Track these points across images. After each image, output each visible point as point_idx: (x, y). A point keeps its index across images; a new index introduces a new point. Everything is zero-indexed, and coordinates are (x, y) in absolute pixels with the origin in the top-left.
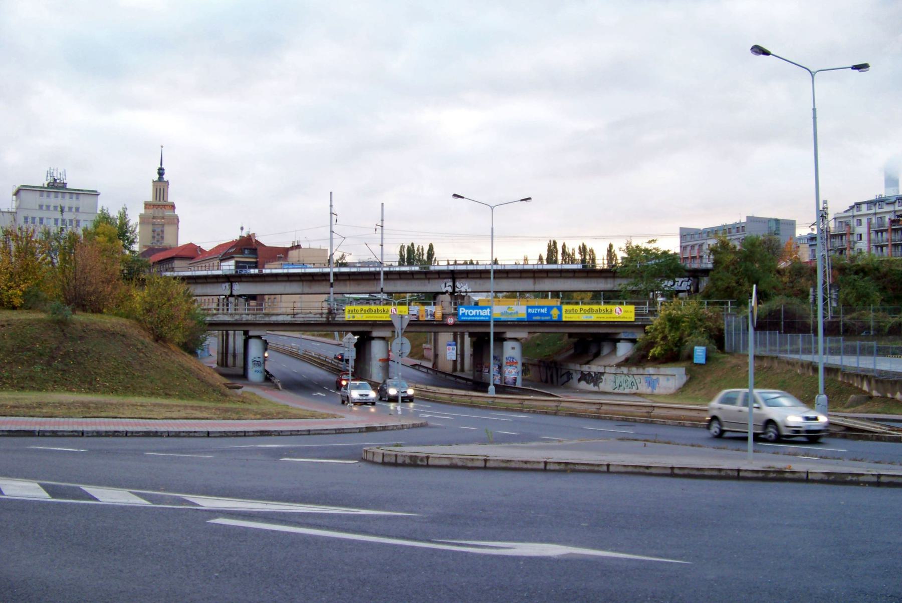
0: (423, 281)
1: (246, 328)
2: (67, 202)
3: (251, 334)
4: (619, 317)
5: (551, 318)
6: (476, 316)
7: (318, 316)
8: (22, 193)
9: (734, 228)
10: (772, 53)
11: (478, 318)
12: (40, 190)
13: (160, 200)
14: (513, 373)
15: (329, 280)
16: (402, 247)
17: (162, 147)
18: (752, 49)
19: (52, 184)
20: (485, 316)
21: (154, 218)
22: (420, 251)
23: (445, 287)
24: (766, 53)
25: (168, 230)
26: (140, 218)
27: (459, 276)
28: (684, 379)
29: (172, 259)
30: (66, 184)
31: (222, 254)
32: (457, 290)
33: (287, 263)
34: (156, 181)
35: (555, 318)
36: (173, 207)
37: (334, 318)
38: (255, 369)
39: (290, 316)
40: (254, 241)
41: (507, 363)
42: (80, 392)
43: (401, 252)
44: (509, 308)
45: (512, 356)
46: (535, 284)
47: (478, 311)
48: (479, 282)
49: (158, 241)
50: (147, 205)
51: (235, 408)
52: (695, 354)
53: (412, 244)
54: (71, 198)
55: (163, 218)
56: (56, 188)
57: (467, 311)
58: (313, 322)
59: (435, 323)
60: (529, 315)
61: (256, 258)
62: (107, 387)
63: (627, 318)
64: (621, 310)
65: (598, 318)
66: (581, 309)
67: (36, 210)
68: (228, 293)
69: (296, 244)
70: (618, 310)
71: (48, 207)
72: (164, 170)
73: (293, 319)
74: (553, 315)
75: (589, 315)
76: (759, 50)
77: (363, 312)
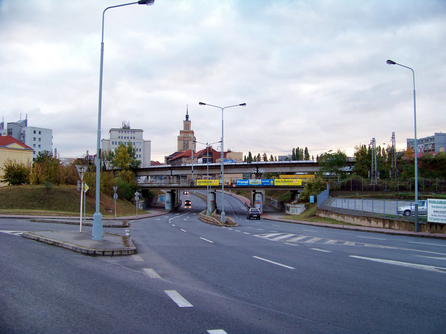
0: (245, 169)
1: (254, 189)
2: (130, 135)
3: (257, 191)
4: (296, 184)
5: (270, 184)
6: (243, 184)
7: (187, 184)
8: (111, 132)
9: (421, 140)
10: (396, 63)
11: (244, 185)
12: (119, 130)
13: (187, 130)
14: (259, 206)
15: (192, 169)
16: (294, 149)
17: (187, 105)
18: (387, 62)
19: (124, 128)
20: (246, 184)
21: (184, 138)
22: (302, 151)
23: (254, 171)
24: (394, 63)
25: (191, 143)
26: (178, 138)
27: (259, 166)
28: (304, 209)
29: (181, 157)
30: (130, 127)
31: (198, 155)
32: (259, 172)
33: (424, 144)
34: (185, 121)
35: (272, 184)
36: (193, 132)
37: (193, 185)
38: (167, 205)
39: (178, 184)
40: (211, 149)
41: (256, 202)
42: (45, 210)
43: (293, 151)
44: (255, 180)
45: (258, 200)
46: (291, 169)
47: (244, 182)
48: (268, 168)
49: (186, 148)
50: (181, 132)
51: (78, 214)
52: (310, 199)
53: (298, 148)
54: (131, 133)
55: (188, 138)
56: (126, 129)
57: (240, 182)
58: (186, 186)
59: (229, 186)
60: (262, 183)
61: (212, 157)
62: (55, 208)
63: (299, 184)
64: (296, 181)
65: (288, 184)
66: (281, 181)
67: (117, 138)
68: (170, 174)
69: (229, 150)
70: (295, 181)
71: (122, 137)
72: (188, 116)
73: (179, 185)
74: (271, 183)
75: (284, 183)
76: (390, 62)
77: (203, 182)
